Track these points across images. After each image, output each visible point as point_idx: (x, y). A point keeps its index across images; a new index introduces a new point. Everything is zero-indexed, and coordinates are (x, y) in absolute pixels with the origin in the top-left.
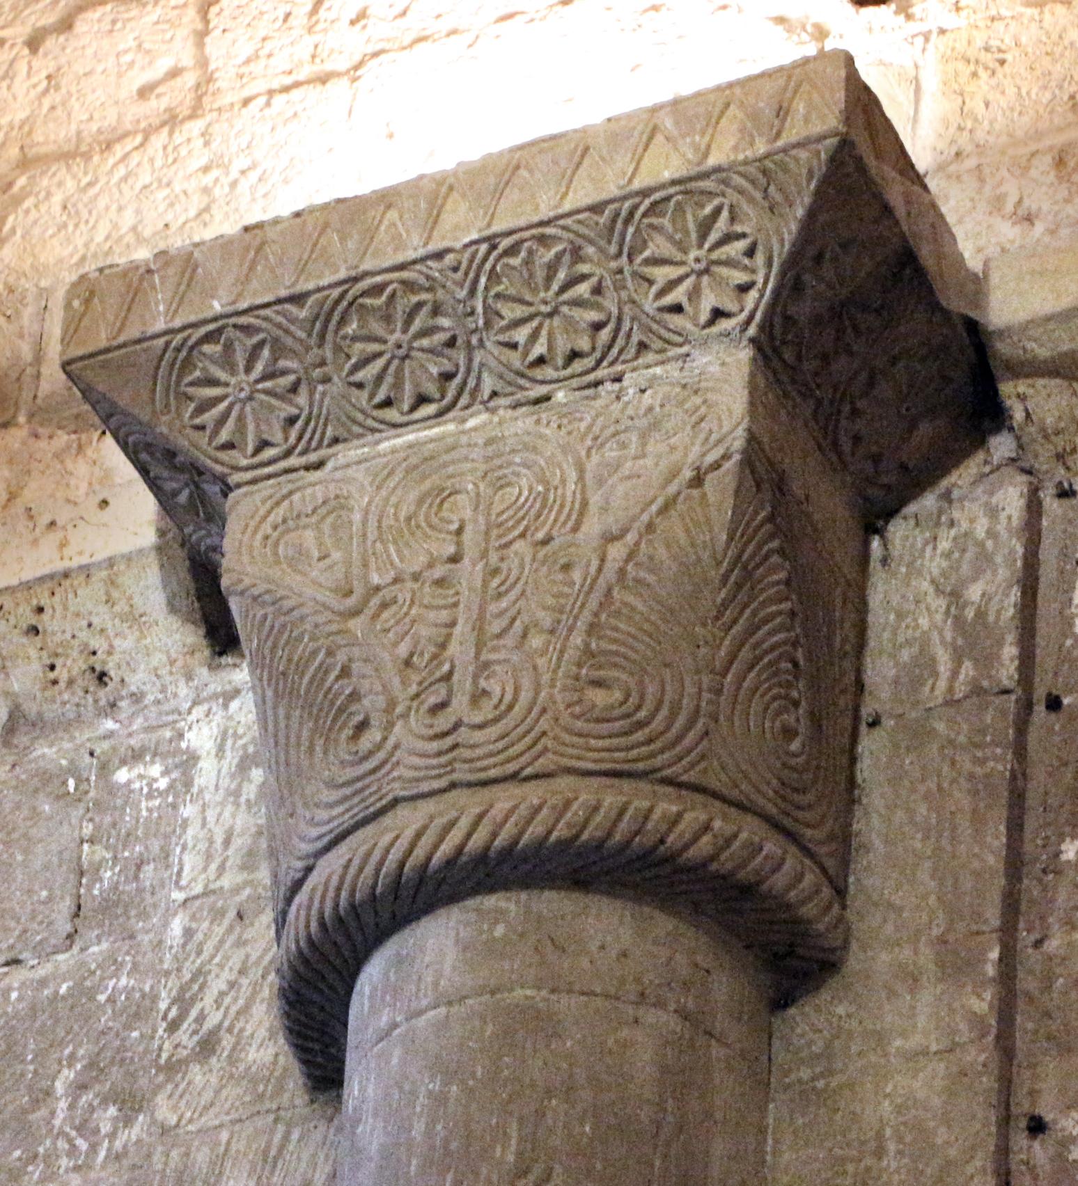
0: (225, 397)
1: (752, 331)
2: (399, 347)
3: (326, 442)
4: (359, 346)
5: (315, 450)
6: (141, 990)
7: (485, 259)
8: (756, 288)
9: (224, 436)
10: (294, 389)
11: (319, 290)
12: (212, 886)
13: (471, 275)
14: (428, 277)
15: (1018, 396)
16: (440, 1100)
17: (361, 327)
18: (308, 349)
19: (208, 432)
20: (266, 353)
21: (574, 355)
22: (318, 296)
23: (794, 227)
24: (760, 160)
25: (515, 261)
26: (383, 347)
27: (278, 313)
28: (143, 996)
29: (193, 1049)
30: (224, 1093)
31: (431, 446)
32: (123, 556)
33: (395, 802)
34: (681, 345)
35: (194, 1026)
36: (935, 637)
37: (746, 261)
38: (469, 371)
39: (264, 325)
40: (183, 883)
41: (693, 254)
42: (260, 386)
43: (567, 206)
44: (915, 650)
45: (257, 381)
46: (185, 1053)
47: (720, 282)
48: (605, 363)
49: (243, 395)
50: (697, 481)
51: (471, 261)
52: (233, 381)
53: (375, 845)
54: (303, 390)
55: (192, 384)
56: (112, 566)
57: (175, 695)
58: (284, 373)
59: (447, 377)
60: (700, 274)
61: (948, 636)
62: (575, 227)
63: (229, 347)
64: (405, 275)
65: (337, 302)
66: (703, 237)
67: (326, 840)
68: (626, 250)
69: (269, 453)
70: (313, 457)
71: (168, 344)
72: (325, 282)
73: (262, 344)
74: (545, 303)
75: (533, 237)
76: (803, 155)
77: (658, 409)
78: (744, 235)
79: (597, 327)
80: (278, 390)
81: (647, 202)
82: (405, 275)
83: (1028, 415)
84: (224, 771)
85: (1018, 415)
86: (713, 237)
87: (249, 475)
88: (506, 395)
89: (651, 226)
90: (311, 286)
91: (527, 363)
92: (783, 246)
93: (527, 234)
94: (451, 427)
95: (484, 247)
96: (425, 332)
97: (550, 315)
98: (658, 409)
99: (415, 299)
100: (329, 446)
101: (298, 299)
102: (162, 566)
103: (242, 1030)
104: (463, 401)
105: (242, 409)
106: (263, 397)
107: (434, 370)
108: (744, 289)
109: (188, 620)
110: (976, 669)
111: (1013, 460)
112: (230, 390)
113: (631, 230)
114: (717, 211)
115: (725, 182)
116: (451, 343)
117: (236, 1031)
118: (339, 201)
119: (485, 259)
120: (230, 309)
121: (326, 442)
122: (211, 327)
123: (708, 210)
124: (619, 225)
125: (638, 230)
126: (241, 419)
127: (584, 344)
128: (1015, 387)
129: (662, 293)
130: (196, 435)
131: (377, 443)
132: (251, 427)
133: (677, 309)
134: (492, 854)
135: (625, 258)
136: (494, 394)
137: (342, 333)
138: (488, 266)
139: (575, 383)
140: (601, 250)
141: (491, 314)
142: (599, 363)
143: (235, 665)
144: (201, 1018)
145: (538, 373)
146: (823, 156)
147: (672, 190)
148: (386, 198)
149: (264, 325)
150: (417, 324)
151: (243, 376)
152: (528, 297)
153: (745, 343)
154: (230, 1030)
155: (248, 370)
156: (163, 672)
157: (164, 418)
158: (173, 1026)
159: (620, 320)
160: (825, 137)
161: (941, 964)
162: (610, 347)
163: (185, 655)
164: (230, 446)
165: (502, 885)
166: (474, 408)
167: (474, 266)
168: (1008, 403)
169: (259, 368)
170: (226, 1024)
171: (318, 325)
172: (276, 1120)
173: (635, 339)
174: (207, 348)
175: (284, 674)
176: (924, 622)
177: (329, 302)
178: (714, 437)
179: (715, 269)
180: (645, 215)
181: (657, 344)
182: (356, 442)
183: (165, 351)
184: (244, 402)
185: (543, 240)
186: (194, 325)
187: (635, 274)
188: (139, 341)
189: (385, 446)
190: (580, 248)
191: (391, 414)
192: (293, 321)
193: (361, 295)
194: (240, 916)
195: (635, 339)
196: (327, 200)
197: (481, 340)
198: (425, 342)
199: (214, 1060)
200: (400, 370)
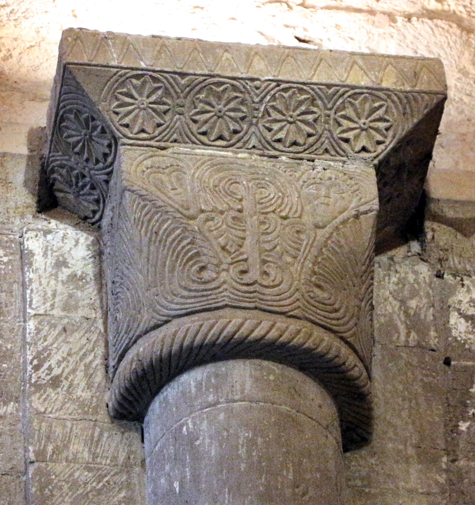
0: (132, 104)
1: (376, 162)
2: (220, 112)
3: (171, 140)
4: (201, 105)
5: (165, 141)
6: (6, 347)
7: (272, 89)
8: (385, 145)
9: (126, 121)
10: (165, 112)
11: (195, 75)
12: (48, 313)
13: (264, 93)
14: (244, 87)
15: (432, 229)
16: (251, 443)
17: (206, 97)
18: (178, 98)
19: (120, 116)
20: (160, 92)
21: (295, 143)
22: (194, 77)
23: (411, 126)
24: (406, 92)
25: (286, 95)
26: (211, 109)
27: (172, 77)
28: (7, 350)
29: (48, 381)
30: (67, 405)
31: (219, 159)
32: (11, 154)
33: (226, 306)
34: (342, 156)
35: (46, 371)
36: (395, 317)
37: (385, 132)
38: (246, 133)
39: (164, 80)
40: (33, 306)
41: (363, 121)
42: (151, 106)
43: (315, 80)
44: (387, 319)
45: (150, 103)
46: (44, 382)
47: (370, 137)
48: (307, 152)
49: (142, 106)
50: (357, 217)
51: (266, 88)
52: (140, 99)
53: (230, 321)
54: (170, 114)
55: (121, 93)
56: (4, 157)
57: (13, 223)
58: (164, 104)
59: (235, 132)
60: (363, 130)
61: (403, 319)
62: (318, 90)
63: (144, 83)
64: (235, 82)
65: (200, 83)
66: (369, 115)
67: (184, 312)
68: (335, 107)
69: (144, 135)
70: (162, 144)
71: (117, 72)
72: (199, 72)
73: (159, 88)
74: (291, 117)
75: (297, 88)
76: (426, 97)
77: (333, 179)
78: (388, 121)
79: (310, 135)
80: (158, 110)
81: (352, 92)
82: (235, 82)
83: (433, 238)
84: (48, 264)
85: (429, 236)
86: (375, 116)
87: (131, 142)
88: (259, 149)
89: (350, 102)
90: (191, 71)
91: (273, 139)
92: (403, 130)
93: (295, 85)
94: (230, 154)
95: (274, 84)
96: (234, 110)
97: (291, 123)
98: (333, 179)
99: (236, 94)
100: (171, 142)
101: (183, 75)
102: (28, 165)
103: (72, 380)
104: (239, 144)
105: (139, 112)
106: (150, 110)
107: (232, 128)
108: (379, 143)
109: (31, 192)
110: (418, 336)
111: (419, 254)
112: (136, 102)
113: (341, 101)
114: (381, 106)
115: (389, 96)
116: (243, 119)
117: (70, 380)
118: (200, 40)
119: (272, 89)
120: (149, 68)
121: (171, 140)
122: (140, 72)
123: (376, 105)
124: (336, 97)
125: (343, 102)
126: (137, 116)
127: (301, 140)
128: (432, 225)
129: (343, 132)
130: (113, 116)
131: (194, 149)
132: (140, 121)
133: (347, 141)
134: (277, 344)
135: (333, 111)
136: (254, 147)
137: (197, 96)
138: (273, 92)
139: (291, 155)
140: (325, 105)
141: (267, 112)
142: (305, 150)
143: (45, 219)
144: (50, 369)
145: (277, 145)
146: (435, 101)
147: (365, 91)
148: (226, 47)
149: (164, 80)
150: (232, 105)
151: (145, 99)
152: (285, 112)
153: (372, 165)
154: (66, 378)
155: (148, 97)
156: (11, 211)
157: (103, 103)
158: (37, 368)
159: (320, 137)
160: (438, 93)
161: (419, 455)
162: (312, 146)
163: (24, 206)
164: (127, 126)
165: (280, 360)
166: (243, 150)
167: (267, 90)
168: (427, 230)
169: (153, 98)
170: (64, 375)
171: (188, 89)
172: (95, 425)
173: (324, 147)
174: (134, 81)
175: (156, 233)
176: (389, 308)
177: (197, 81)
178: (363, 200)
179: (372, 131)
180: (349, 97)
181: (333, 153)
182: (184, 145)
183: (115, 74)
184: (141, 109)
185: (301, 90)
186: (132, 69)
187: (335, 120)
188: (105, 66)
189: (198, 151)
190: (315, 100)
191: (204, 139)
192: (177, 84)
193: (212, 84)
194: (65, 330)
195: (324, 147)
196: (194, 38)
197: (257, 122)
198: (232, 114)
199: (59, 389)
200: (215, 122)
